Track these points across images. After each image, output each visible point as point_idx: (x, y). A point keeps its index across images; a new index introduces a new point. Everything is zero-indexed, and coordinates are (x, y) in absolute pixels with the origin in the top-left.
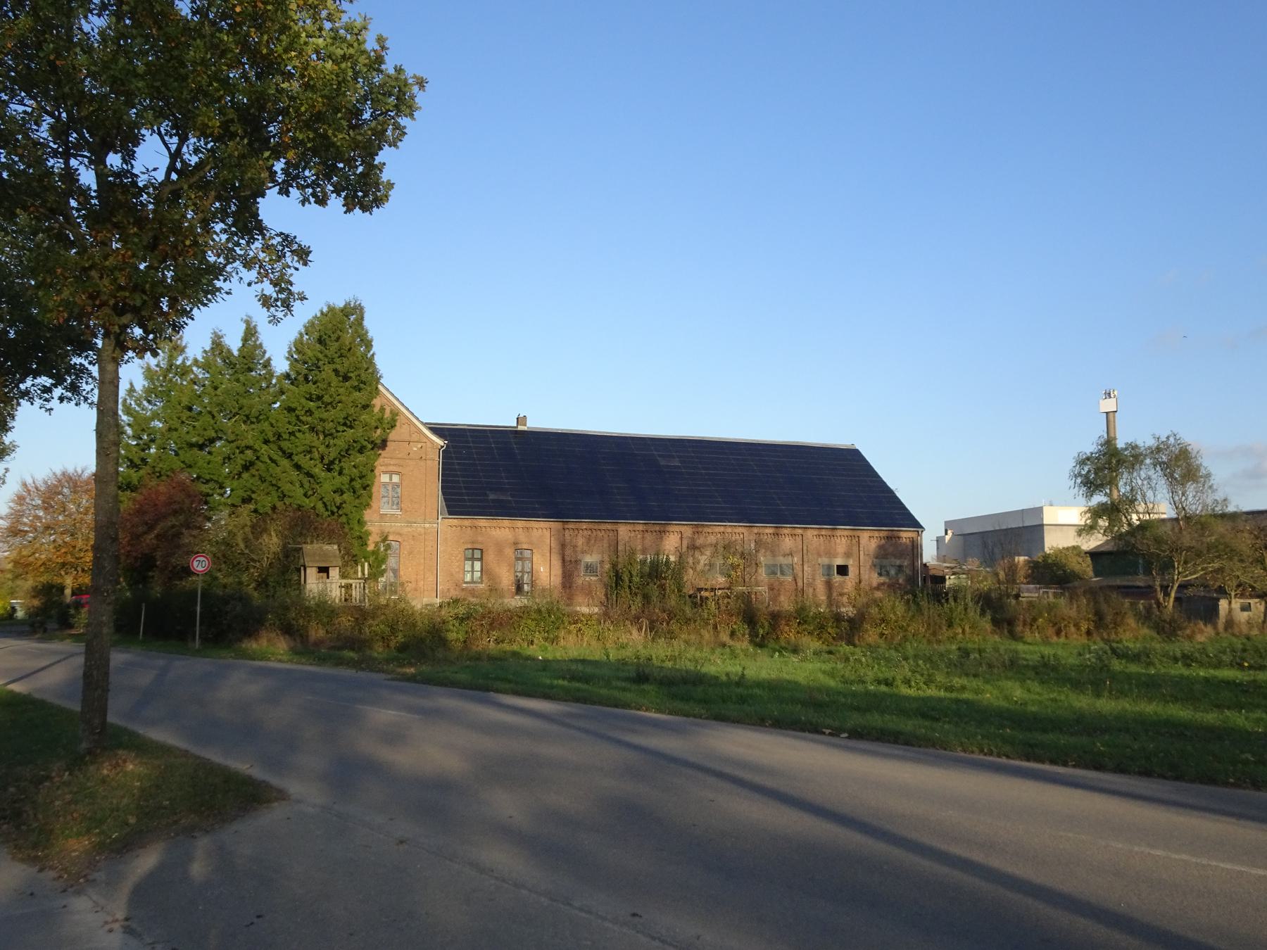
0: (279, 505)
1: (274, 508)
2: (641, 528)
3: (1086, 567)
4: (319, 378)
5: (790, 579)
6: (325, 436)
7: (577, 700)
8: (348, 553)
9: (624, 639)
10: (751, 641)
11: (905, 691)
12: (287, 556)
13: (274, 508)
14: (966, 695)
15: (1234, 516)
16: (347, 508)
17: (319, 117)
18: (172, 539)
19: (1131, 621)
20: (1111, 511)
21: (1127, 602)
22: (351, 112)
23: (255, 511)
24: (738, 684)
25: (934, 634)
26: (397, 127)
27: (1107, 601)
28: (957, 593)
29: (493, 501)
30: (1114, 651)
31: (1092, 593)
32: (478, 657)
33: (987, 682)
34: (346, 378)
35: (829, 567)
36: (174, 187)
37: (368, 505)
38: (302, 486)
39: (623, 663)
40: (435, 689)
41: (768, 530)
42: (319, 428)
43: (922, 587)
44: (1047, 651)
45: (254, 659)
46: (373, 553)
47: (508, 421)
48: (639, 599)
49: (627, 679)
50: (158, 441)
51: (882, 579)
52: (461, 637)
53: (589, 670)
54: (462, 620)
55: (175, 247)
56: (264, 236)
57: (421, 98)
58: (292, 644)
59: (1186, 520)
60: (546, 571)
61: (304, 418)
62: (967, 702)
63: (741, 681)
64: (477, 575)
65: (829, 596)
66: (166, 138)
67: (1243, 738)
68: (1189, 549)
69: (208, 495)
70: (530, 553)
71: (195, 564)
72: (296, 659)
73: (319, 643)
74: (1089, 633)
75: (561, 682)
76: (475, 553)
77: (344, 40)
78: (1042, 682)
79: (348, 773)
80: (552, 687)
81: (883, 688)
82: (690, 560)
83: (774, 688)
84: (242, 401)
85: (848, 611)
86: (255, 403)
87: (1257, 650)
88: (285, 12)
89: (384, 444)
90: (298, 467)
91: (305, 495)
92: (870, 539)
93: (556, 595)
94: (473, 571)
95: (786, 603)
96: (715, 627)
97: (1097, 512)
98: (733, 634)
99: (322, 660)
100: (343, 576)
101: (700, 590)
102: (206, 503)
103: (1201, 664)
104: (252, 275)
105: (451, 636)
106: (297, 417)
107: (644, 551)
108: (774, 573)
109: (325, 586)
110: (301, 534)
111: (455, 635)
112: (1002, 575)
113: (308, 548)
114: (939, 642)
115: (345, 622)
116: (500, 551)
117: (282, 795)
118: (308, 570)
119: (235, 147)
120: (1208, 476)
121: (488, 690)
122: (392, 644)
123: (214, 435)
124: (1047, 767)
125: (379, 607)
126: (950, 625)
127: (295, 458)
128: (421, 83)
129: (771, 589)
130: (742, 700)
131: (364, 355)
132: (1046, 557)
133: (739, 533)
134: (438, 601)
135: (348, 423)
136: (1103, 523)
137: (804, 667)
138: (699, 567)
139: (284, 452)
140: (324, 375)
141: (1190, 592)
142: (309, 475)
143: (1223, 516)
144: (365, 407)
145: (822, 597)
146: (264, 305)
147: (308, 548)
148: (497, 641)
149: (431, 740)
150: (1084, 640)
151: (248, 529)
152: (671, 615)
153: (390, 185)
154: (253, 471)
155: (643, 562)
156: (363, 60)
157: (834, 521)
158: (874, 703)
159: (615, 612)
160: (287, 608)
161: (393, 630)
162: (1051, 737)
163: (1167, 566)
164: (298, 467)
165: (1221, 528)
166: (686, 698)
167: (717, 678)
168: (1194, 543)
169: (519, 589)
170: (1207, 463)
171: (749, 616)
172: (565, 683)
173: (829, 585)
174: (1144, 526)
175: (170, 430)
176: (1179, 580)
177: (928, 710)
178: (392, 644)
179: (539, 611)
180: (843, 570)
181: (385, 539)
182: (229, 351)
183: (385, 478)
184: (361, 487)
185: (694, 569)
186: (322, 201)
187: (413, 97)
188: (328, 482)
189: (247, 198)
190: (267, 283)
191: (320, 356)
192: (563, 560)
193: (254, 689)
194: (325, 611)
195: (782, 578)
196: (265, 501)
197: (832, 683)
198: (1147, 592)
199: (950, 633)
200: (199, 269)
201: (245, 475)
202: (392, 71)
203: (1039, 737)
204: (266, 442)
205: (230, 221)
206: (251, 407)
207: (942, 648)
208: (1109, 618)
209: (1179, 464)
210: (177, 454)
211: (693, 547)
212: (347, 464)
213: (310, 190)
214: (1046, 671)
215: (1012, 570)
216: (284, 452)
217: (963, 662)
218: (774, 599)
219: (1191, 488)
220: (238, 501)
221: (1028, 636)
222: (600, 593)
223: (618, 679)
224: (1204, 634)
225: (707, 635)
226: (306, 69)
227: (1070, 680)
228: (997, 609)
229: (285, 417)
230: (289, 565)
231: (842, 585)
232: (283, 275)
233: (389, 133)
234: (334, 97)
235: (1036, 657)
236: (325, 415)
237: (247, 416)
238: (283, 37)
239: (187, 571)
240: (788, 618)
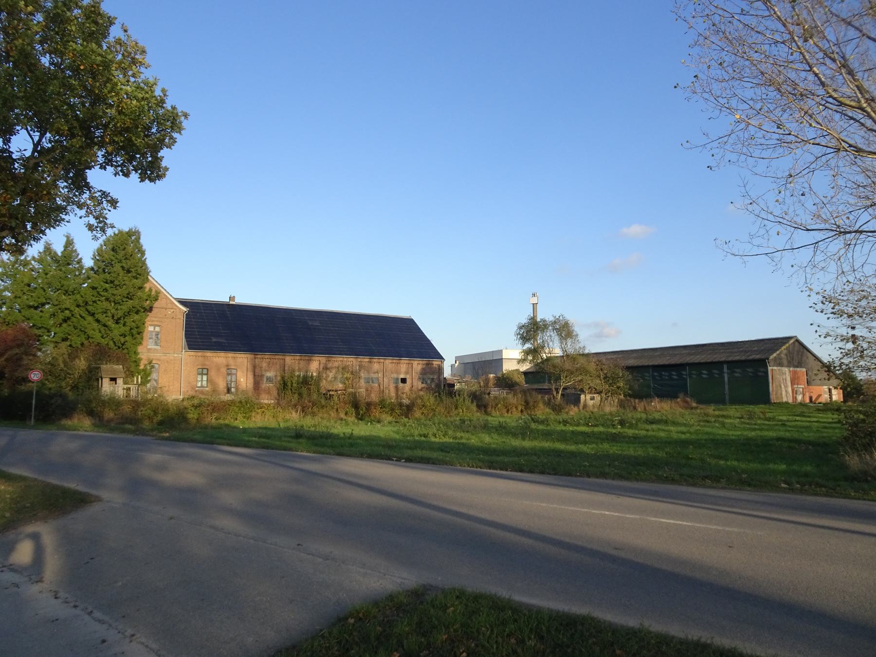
0: (86, 342)
1: (82, 344)
2: (298, 358)
3: (521, 380)
4: (112, 270)
5: (376, 385)
6: (115, 303)
7: (264, 448)
8: (128, 370)
9: (288, 417)
10: (357, 417)
11: (433, 439)
12: (90, 372)
13: (82, 344)
14: (463, 441)
15: (588, 355)
16: (128, 345)
17: (127, 130)
18: (16, 361)
19: (541, 405)
20: (534, 352)
21: (540, 396)
22: (145, 128)
23: (70, 346)
24: (349, 438)
25: (449, 412)
26: (171, 138)
27: (530, 394)
28: (460, 392)
29: (215, 342)
30: (533, 419)
31: (524, 392)
32: (206, 427)
33: (473, 434)
34: (129, 271)
35: (397, 379)
36: (36, 161)
37: (140, 343)
38: (100, 332)
39: (288, 428)
40: (182, 444)
41: (366, 360)
42: (112, 299)
43: (444, 389)
44: (501, 420)
45: (69, 430)
46: (143, 370)
47: (225, 299)
48: (296, 396)
49: (291, 437)
50: (8, 304)
51: (424, 385)
52: (196, 416)
53: (269, 432)
54: (196, 407)
55: (37, 195)
56: (90, 191)
57: (185, 123)
58: (93, 421)
59: (567, 356)
60: (244, 380)
61: (102, 293)
62: (463, 444)
63: (351, 436)
64: (205, 383)
65: (397, 394)
66: (31, 132)
67: (585, 456)
68: (568, 370)
69: (40, 336)
70: (236, 371)
71: (32, 375)
72: (96, 429)
73: (110, 421)
74: (522, 411)
75: (254, 439)
76: (204, 371)
77: (142, 89)
78: (499, 434)
79: (136, 487)
80: (249, 441)
81: (423, 438)
82: (324, 375)
83: (368, 440)
84: (63, 282)
85: (406, 401)
86: (71, 284)
87: (595, 418)
88: (109, 71)
89: (151, 309)
90: (98, 321)
91: (102, 337)
92: (418, 365)
93: (250, 394)
94: (202, 381)
95: (374, 397)
96: (337, 410)
97: (527, 352)
98: (346, 414)
99: (112, 430)
100: (125, 383)
101: (329, 391)
102: (38, 341)
103: (571, 425)
104: (83, 212)
105: (190, 416)
106: (98, 292)
107: (299, 370)
108: (368, 382)
109: (114, 388)
110: (100, 359)
111: (192, 415)
112: (482, 384)
113: (104, 367)
114: (451, 416)
115: (127, 409)
116: (218, 370)
117: (98, 499)
118: (104, 380)
119: (77, 142)
120: (577, 335)
121: (213, 444)
122: (155, 421)
123: (44, 301)
124: (498, 472)
125: (147, 400)
126: (456, 408)
127: (97, 316)
128: (186, 116)
129: (367, 390)
130: (352, 445)
131: (140, 259)
132: (503, 375)
133: (351, 361)
134: (181, 397)
135: (129, 297)
136: (530, 358)
137: (384, 429)
138: (329, 379)
139: (89, 312)
140: (115, 269)
141: (568, 391)
142: (105, 325)
143: (583, 355)
144: (140, 288)
145: (393, 394)
146: (89, 229)
147: (104, 367)
148: (217, 419)
149: (185, 469)
150: (519, 414)
151: (66, 356)
152: (314, 404)
153: (166, 169)
154: (69, 323)
155: (299, 376)
156: (153, 100)
157: (400, 355)
158: (417, 445)
159: (283, 403)
160: (90, 401)
161: (155, 412)
162: (500, 458)
163: (558, 379)
164: (98, 321)
165: (582, 361)
166: (323, 446)
167: (338, 435)
168: (570, 368)
169: (229, 391)
170: (577, 329)
171: (356, 405)
172: (256, 439)
173: (397, 388)
174: (548, 359)
175: (16, 297)
176: (563, 385)
177: (444, 448)
178: (155, 421)
179: (241, 402)
180: (404, 381)
181: (150, 363)
182: (55, 253)
183: (151, 329)
184: (137, 333)
185: (326, 380)
186: (127, 175)
187: (181, 123)
188: (117, 330)
189: (81, 170)
190: (91, 217)
191: (113, 258)
192: (254, 375)
193: (73, 445)
194: (114, 403)
195: (373, 385)
196: (76, 340)
197: (397, 437)
198: (548, 391)
199: (456, 412)
200: (51, 208)
201: (64, 325)
202: (169, 108)
203: (495, 458)
204: (78, 306)
205: (70, 181)
206: (69, 286)
207: (452, 419)
208: (531, 404)
209: (564, 330)
210: (20, 312)
211: (326, 368)
212: (129, 320)
213: (120, 168)
214: (501, 429)
215: (487, 381)
216: (89, 312)
217: (462, 426)
218: (368, 395)
219: (569, 341)
220: (59, 340)
221: (494, 413)
222: (275, 393)
223: (285, 436)
224: (573, 411)
225: (333, 414)
226: (120, 103)
227: (511, 433)
228: (479, 400)
229: (90, 292)
230: (92, 377)
231: (403, 388)
232: (101, 214)
233: (167, 140)
234: (136, 120)
235: (497, 423)
236: (115, 292)
237: (66, 291)
238: (108, 85)
239: (26, 380)
240: (375, 405)
